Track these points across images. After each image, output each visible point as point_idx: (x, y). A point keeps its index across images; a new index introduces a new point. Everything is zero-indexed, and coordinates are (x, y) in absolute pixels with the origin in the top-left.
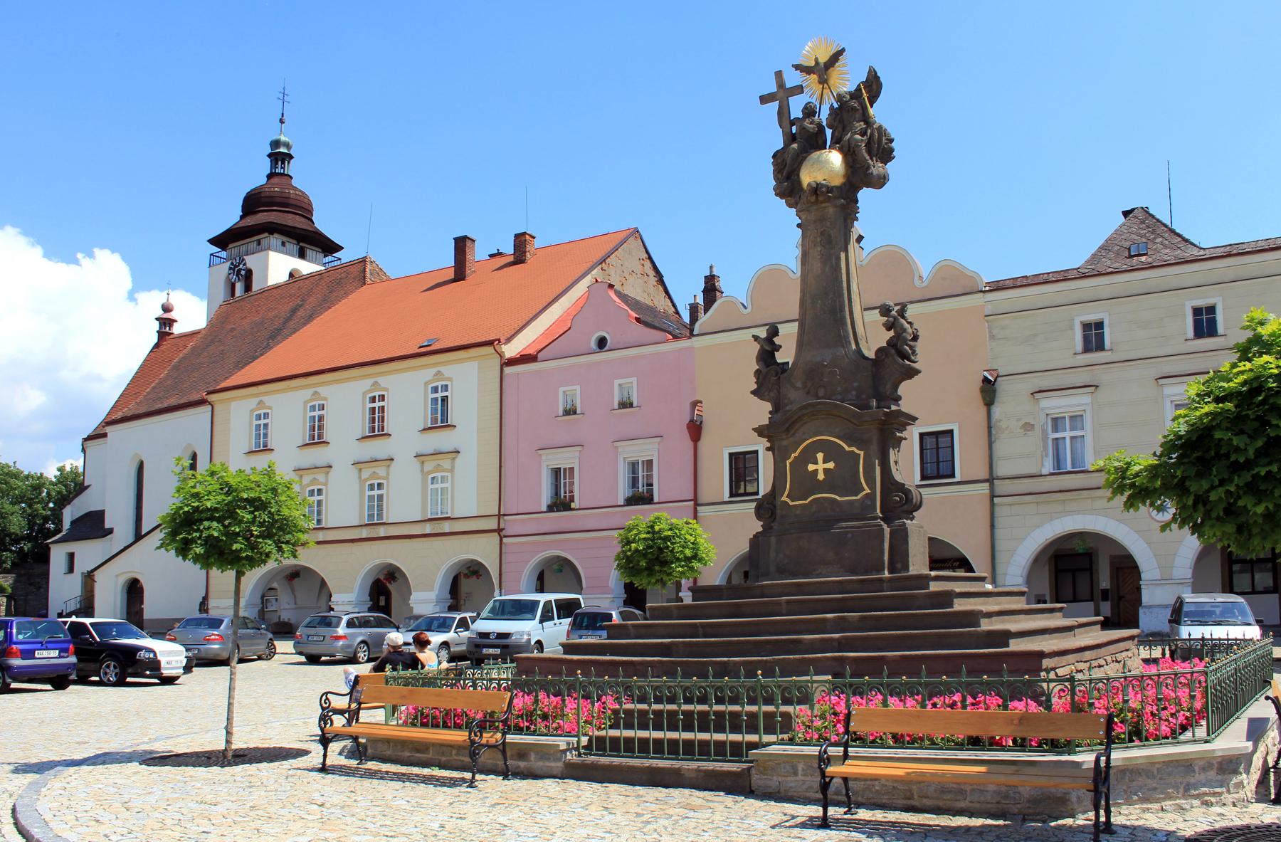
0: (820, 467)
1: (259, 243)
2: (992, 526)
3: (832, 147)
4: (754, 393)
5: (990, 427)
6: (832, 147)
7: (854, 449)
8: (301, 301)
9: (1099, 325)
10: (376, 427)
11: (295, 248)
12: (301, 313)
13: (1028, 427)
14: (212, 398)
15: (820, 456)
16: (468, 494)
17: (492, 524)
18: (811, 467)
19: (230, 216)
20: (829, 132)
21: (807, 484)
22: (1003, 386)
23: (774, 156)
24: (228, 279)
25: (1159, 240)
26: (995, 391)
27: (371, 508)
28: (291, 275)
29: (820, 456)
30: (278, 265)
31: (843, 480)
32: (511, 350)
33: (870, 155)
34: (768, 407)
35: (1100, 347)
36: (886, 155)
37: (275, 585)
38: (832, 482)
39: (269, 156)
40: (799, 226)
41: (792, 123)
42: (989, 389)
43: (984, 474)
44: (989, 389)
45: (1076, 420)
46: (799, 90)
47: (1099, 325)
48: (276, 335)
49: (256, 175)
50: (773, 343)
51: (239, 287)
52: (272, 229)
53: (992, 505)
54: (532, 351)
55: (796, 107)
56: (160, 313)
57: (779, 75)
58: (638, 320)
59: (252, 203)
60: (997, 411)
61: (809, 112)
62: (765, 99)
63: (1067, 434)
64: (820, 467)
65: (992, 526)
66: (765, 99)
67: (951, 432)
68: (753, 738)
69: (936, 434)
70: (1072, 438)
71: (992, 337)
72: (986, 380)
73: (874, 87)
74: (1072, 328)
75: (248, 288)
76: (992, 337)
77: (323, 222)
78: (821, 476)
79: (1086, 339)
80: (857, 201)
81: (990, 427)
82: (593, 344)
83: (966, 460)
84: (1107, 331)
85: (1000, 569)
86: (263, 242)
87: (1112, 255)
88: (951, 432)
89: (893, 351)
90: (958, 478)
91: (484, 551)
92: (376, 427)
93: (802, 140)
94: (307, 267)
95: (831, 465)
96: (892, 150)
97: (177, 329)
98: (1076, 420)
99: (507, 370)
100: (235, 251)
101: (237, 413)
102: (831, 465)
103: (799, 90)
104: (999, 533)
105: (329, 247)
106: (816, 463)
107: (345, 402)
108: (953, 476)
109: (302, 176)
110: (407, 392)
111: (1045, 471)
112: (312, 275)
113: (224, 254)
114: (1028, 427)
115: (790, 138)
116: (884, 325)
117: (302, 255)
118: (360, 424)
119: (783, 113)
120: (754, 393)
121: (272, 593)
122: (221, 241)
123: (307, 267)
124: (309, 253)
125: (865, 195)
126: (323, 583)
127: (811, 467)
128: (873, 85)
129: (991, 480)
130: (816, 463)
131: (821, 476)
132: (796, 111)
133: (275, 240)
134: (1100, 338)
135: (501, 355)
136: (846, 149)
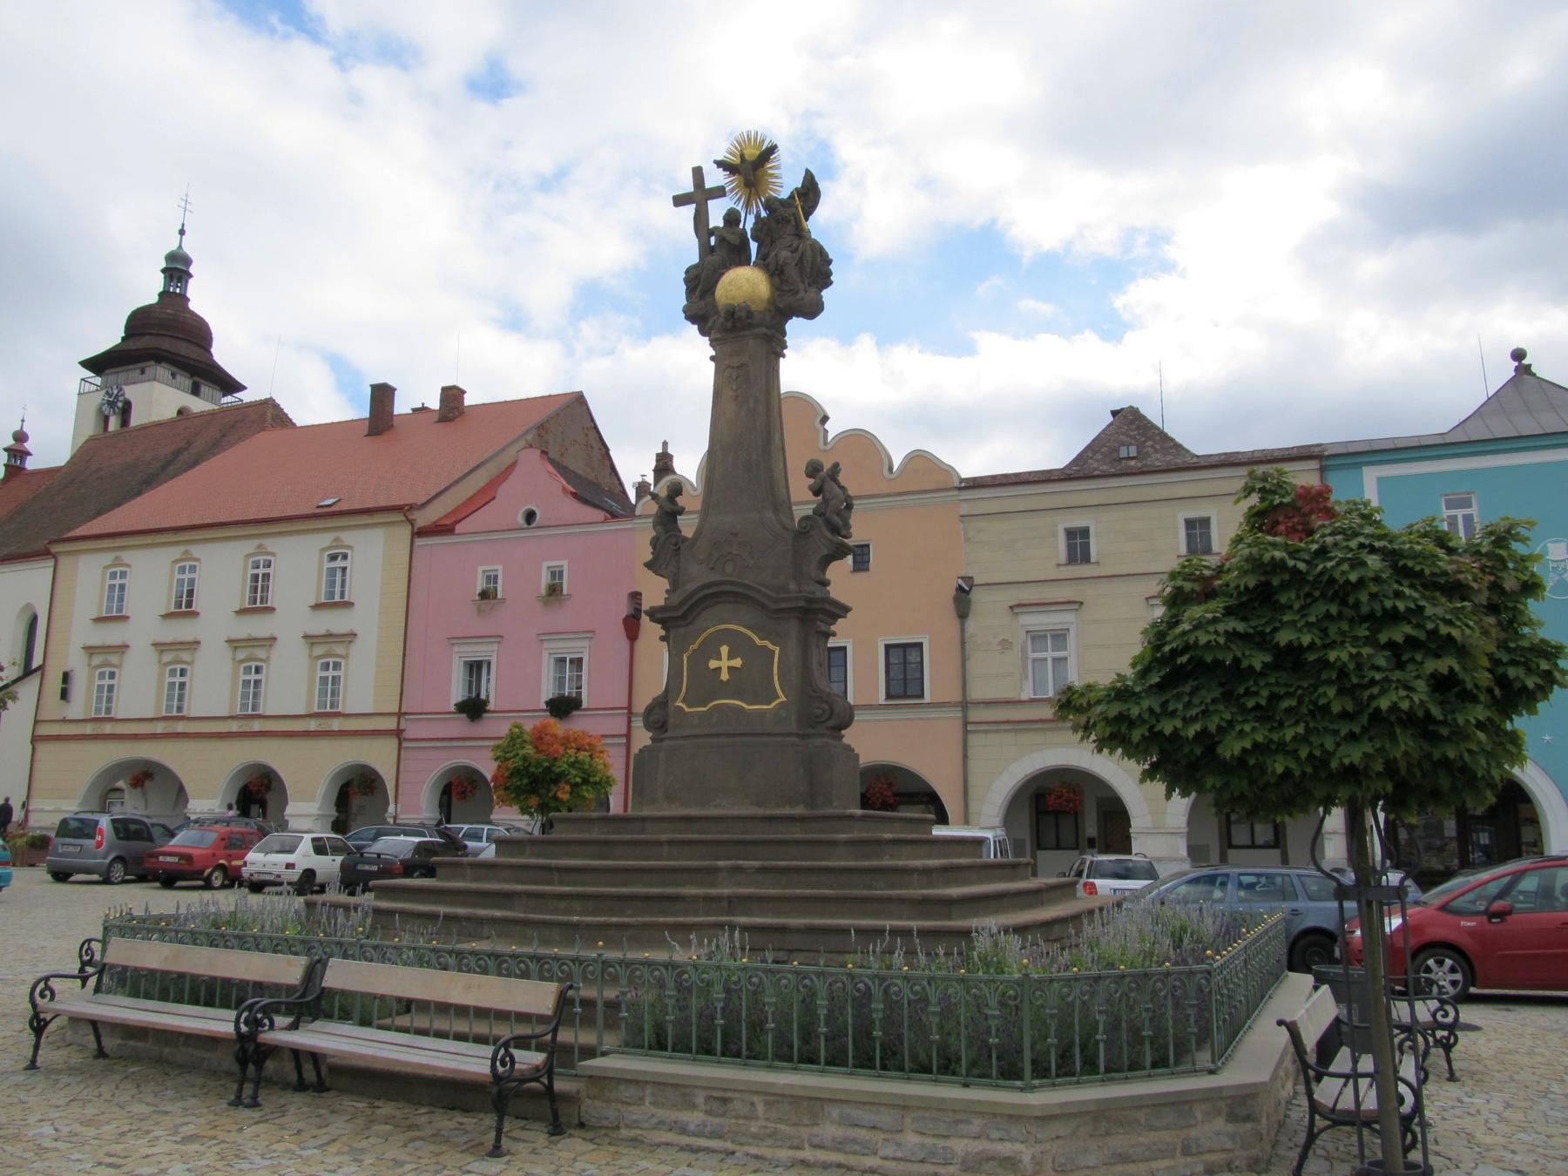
0: (724, 663)
1: (143, 372)
2: (965, 757)
3: (760, 258)
4: (649, 565)
5: (963, 643)
6: (760, 258)
7: (767, 643)
8: (184, 447)
9: (1085, 532)
10: (258, 602)
11: (188, 382)
12: (184, 457)
13: (1006, 645)
14: (55, 549)
15: (724, 650)
16: (365, 687)
17: (390, 724)
18: (713, 664)
19: (111, 336)
20: (754, 246)
21: (706, 685)
22: (976, 595)
23: (687, 272)
24: (100, 410)
25: (1149, 443)
26: (969, 602)
27: (245, 696)
28: (180, 412)
29: (724, 650)
30: (159, 399)
31: (749, 683)
32: (424, 518)
33: (802, 277)
34: (664, 584)
35: (1086, 559)
36: (822, 278)
37: (121, 784)
38: (739, 684)
39: (164, 271)
40: (712, 358)
41: (711, 232)
42: (963, 597)
43: (957, 697)
44: (963, 597)
45: (1060, 637)
46: (719, 192)
47: (1085, 532)
48: (149, 481)
49: (148, 289)
50: (675, 504)
51: (114, 423)
52: (159, 357)
53: (966, 732)
54: (448, 521)
55: (716, 215)
56: (10, 442)
57: (698, 173)
58: (574, 495)
59: (139, 322)
60: (972, 624)
61: (732, 218)
62: (679, 201)
63: (1050, 654)
64: (724, 663)
65: (965, 757)
66: (679, 201)
67: (920, 645)
68: (587, 1038)
69: (905, 647)
70: (1055, 660)
71: (967, 540)
72: (960, 588)
73: (811, 195)
74: (1054, 535)
75: (125, 422)
76: (967, 540)
77: (224, 354)
78: (725, 676)
79: (1071, 549)
80: (784, 334)
81: (963, 643)
82: (521, 520)
83: (936, 680)
84: (1093, 541)
85: (973, 808)
86: (148, 371)
87: (1099, 456)
88: (920, 645)
89: (820, 521)
90: (927, 698)
91: (380, 757)
92: (258, 602)
93: (721, 249)
94: (198, 405)
95: (737, 663)
96: (830, 274)
97: (31, 464)
98: (1060, 637)
99: (419, 542)
100: (112, 379)
101: (87, 574)
102: (737, 663)
103: (719, 192)
104: (973, 765)
105: (230, 385)
106: (720, 659)
107: (222, 569)
108: (921, 696)
109: (201, 299)
110: (297, 562)
111: (1024, 697)
112: (202, 415)
113: (98, 381)
114: (1006, 645)
115: (705, 250)
116: (811, 488)
117: (195, 391)
118: (238, 595)
119: (700, 219)
120: (649, 565)
121: (117, 794)
122: (96, 364)
123: (198, 405)
124: (204, 389)
125: (794, 326)
126: (181, 789)
127: (713, 664)
128: (809, 193)
129: (965, 705)
130: (720, 659)
131: (725, 676)
132: (716, 220)
133: (163, 371)
134: (1086, 548)
135: (412, 523)
136: (772, 267)
